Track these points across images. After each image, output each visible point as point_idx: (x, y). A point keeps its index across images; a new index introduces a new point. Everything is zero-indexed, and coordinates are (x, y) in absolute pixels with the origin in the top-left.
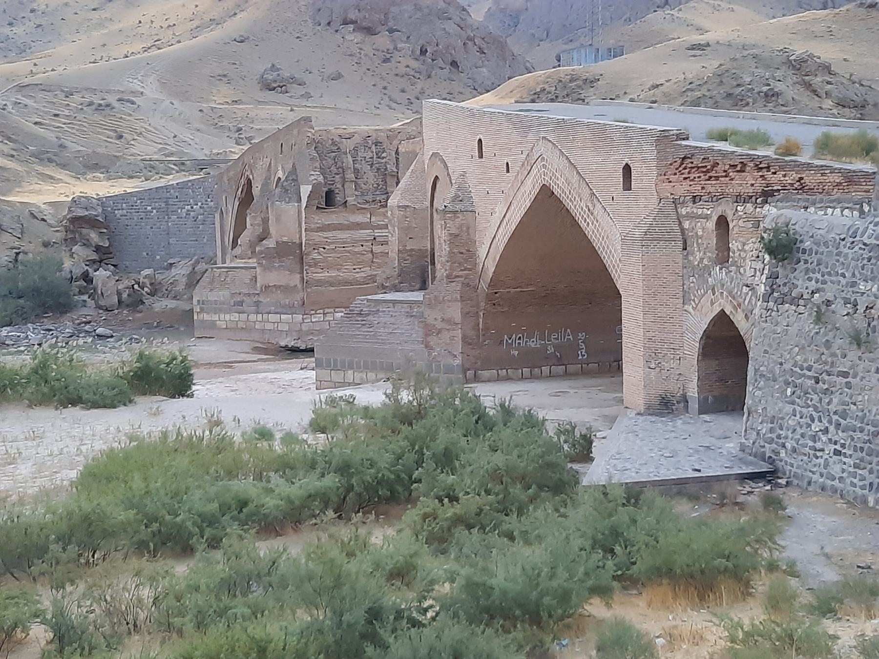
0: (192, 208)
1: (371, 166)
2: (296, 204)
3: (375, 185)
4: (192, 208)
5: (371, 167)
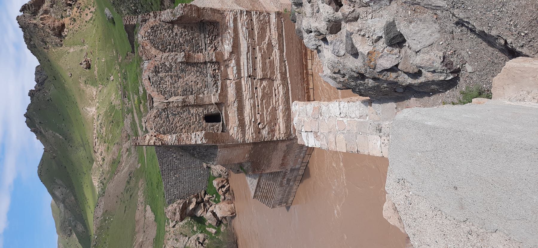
0: (175, 158)
2: (219, 150)
4: (175, 158)
5: (180, 77)
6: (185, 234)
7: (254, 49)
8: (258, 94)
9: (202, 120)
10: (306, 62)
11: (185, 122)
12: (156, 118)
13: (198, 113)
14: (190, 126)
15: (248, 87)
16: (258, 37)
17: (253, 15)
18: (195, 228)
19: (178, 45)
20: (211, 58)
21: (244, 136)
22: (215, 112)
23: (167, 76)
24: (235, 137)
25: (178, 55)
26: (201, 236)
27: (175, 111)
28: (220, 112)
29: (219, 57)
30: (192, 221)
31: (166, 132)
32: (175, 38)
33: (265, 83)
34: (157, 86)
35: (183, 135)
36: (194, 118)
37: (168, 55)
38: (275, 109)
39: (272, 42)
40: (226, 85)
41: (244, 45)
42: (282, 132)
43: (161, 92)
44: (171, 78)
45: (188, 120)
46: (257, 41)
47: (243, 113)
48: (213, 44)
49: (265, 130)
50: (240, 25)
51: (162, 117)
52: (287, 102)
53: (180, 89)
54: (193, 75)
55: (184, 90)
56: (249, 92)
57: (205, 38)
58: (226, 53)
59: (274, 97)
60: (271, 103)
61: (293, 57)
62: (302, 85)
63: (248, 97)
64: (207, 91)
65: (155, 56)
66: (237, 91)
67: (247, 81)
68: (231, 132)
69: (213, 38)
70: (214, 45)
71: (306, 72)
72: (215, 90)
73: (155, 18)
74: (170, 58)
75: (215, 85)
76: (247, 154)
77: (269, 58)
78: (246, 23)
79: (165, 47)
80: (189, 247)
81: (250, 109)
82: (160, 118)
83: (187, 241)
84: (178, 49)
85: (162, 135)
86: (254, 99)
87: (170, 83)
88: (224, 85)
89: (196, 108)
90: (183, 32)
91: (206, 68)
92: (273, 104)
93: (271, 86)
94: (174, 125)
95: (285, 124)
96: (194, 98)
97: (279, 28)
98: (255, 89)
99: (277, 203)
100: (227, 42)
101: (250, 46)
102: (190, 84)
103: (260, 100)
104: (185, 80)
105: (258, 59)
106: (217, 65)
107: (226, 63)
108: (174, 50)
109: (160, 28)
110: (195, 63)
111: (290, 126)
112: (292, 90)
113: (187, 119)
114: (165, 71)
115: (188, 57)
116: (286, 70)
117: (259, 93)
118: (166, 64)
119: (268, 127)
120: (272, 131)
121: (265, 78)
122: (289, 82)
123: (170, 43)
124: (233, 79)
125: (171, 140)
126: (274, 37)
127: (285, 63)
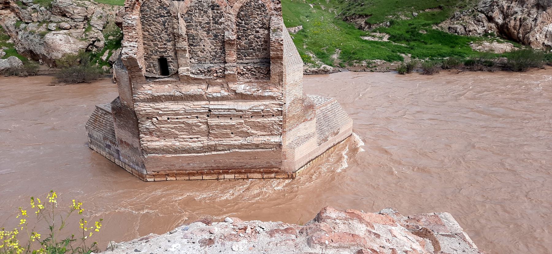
1: (208, 31)
3: (213, 53)
5: (208, 33)
6: (107, 26)
7: (241, 117)
8: (190, 119)
9: (161, 55)
10: (232, 173)
11: (157, 35)
12: (159, 2)
13: (168, 50)
14: (152, 41)
15: (198, 109)
16: (254, 122)
17: (279, 117)
18: (111, 38)
19: (245, 33)
20: (228, 69)
21: (144, 101)
22: (170, 69)
23: (208, 18)
24: (140, 91)
25: (232, 32)
26: (101, 44)
27: (168, 25)
28: (170, 75)
29: (231, 78)
30: (119, 35)
31: (143, 13)
32: (254, 31)
33: (204, 127)
34: (197, 6)
35: (134, 32)
36: (162, 46)
37: (232, 21)
38: (176, 137)
39: (251, 137)
40: (200, 84)
41: (244, 106)
42: (149, 143)
43: (190, 11)
44: (207, 23)
45: (159, 39)
46: (249, 120)
47: (170, 102)
48: (247, 72)
49: (151, 125)
50: (267, 102)
51: (161, 10)
52: (184, 151)
53: (195, 32)
54: (212, 48)
55: (194, 36)
56: (192, 109)
57: (254, 63)
58: (236, 86)
59: (189, 137)
60: (182, 133)
61: (235, 159)
62: (205, 167)
63: (187, 108)
64: (194, 62)
65: (232, 7)
66: (192, 96)
67: (204, 107)
68: (147, 87)
69: (252, 73)
70: (246, 73)
71: (220, 173)
72: (193, 71)
73: (274, 10)
74: (229, 23)
75: (199, 72)
76: (126, 103)
77: (232, 133)
78: (269, 109)
79: (243, 19)
80: (91, 30)
81: (173, 109)
82: (159, 7)
83: (98, 28)
84: (241, 32)
85: (139, 9)
86: (185, 115)
87: (201, 21)
88: (201, 81)
89: (173, 49)
90: (261, 39)
91: (220, 63)
92: (181, 135)
93: (200, 133)
94: (152, 23)
95: (158, 147)
96: (182, 47)
97: (265, 145)
98: (196, 116)
99: (90, 132)
100: (247, 88)
101: (242, 113)
102: (201, 44)
103: (184, 121)
104: (205, 38)
105: (229, 121)
106: (222, 75)
107: (225, 85)
108: (241, 28)
109: (264, 14)
110: (224, 50)
111: (157, 153)
112: (197, 156)
113: (161, 38)
114: (214, 17)
115: (230, 43)
116: (220, 151)
117: (192, 120)
118: (223, 19)
119: (154, 128)
120: (150, 133)
121: (209, 127)
122: (206, 154)
123: (248, 24)
124: (207, 92)
125: (129, 18)
126: (256, 139)
127: (227, 150)
